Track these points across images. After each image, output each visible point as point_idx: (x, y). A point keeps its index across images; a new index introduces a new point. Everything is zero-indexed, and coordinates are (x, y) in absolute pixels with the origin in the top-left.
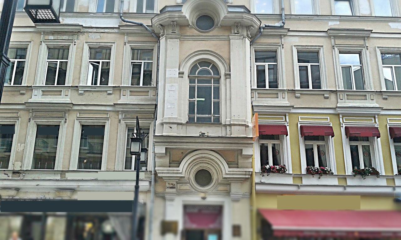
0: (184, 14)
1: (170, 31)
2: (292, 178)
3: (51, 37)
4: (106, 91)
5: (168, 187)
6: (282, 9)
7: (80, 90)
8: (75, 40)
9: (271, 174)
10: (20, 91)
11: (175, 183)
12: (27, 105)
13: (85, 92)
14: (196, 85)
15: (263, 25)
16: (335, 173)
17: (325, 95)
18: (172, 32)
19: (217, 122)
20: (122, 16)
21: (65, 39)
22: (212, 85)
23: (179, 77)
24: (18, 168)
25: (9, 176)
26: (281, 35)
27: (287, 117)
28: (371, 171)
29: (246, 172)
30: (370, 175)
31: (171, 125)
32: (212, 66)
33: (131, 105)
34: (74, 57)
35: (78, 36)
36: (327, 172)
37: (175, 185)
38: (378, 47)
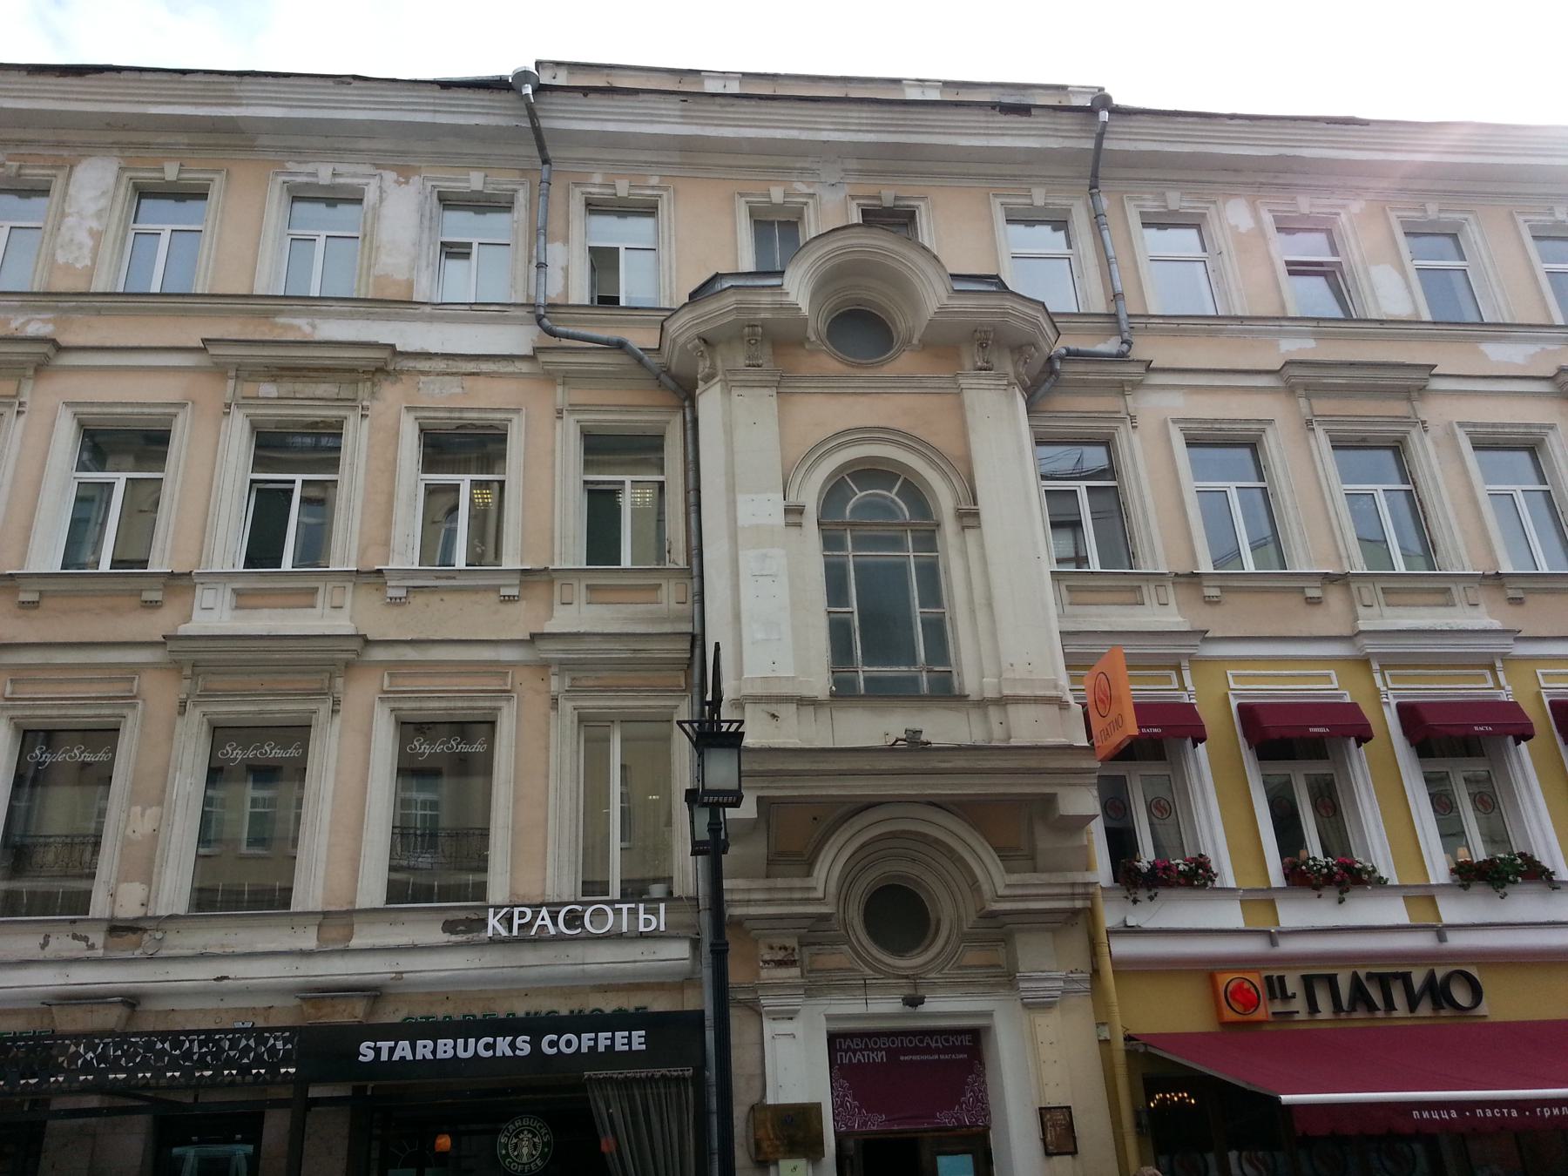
0: (792, 298)
1: (741, 361)
2: (1237, 905)
3: (269, 390)
4: (497, 589)
5: (765, 962)
6: (1116, 297)
7: (393, 587)
8: (363, 400)
9: (1163, 893)
10: (141, 596)
11: (792, 943)
12: (171, 645)
13: (411, 596)
14: (850, 555)
15: (1060, 348)
16: (1394, 880)
17: (1306, 590)
18: (747, 362)
19: (946, 692)
20: (544, 316)
21: (325, 395)
22: (911, 554)
23: (787, 525)
24: (129, 909)
25: (92, 947)
26: (1121, 384)
27: (1186, 675)
28: (1521, 865)
29: (1073, 885)
30: (1520, 879)
31: (773, 708)
32: (900, 487)
33: (599, 638)
34: (361, 462)
35: (374, 384)
36: (1365, 877)
37: (797, 951)
38: (1461, 425)
